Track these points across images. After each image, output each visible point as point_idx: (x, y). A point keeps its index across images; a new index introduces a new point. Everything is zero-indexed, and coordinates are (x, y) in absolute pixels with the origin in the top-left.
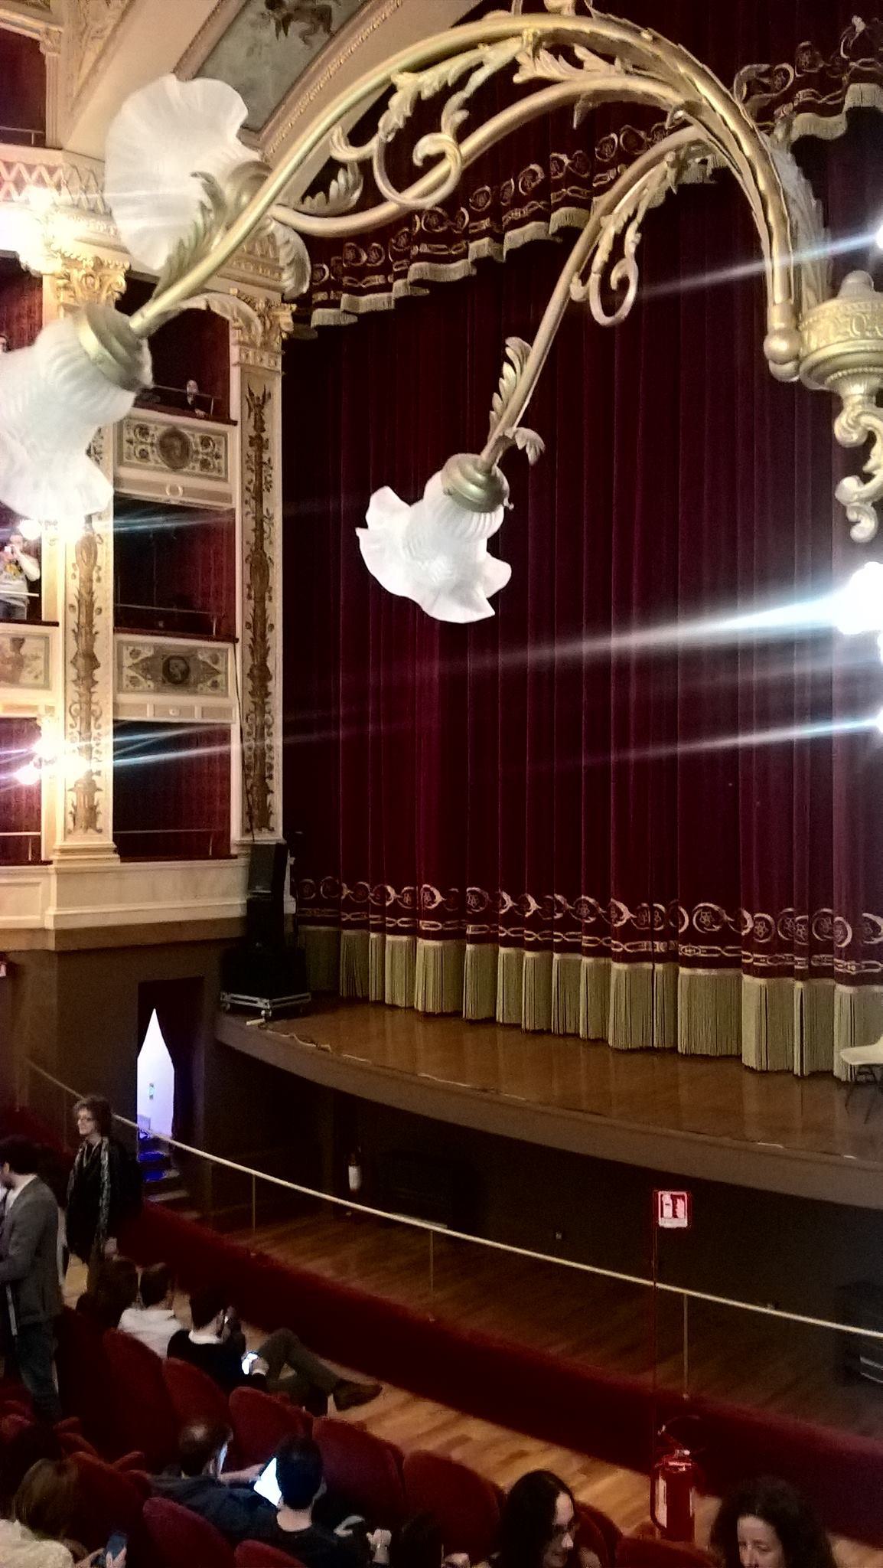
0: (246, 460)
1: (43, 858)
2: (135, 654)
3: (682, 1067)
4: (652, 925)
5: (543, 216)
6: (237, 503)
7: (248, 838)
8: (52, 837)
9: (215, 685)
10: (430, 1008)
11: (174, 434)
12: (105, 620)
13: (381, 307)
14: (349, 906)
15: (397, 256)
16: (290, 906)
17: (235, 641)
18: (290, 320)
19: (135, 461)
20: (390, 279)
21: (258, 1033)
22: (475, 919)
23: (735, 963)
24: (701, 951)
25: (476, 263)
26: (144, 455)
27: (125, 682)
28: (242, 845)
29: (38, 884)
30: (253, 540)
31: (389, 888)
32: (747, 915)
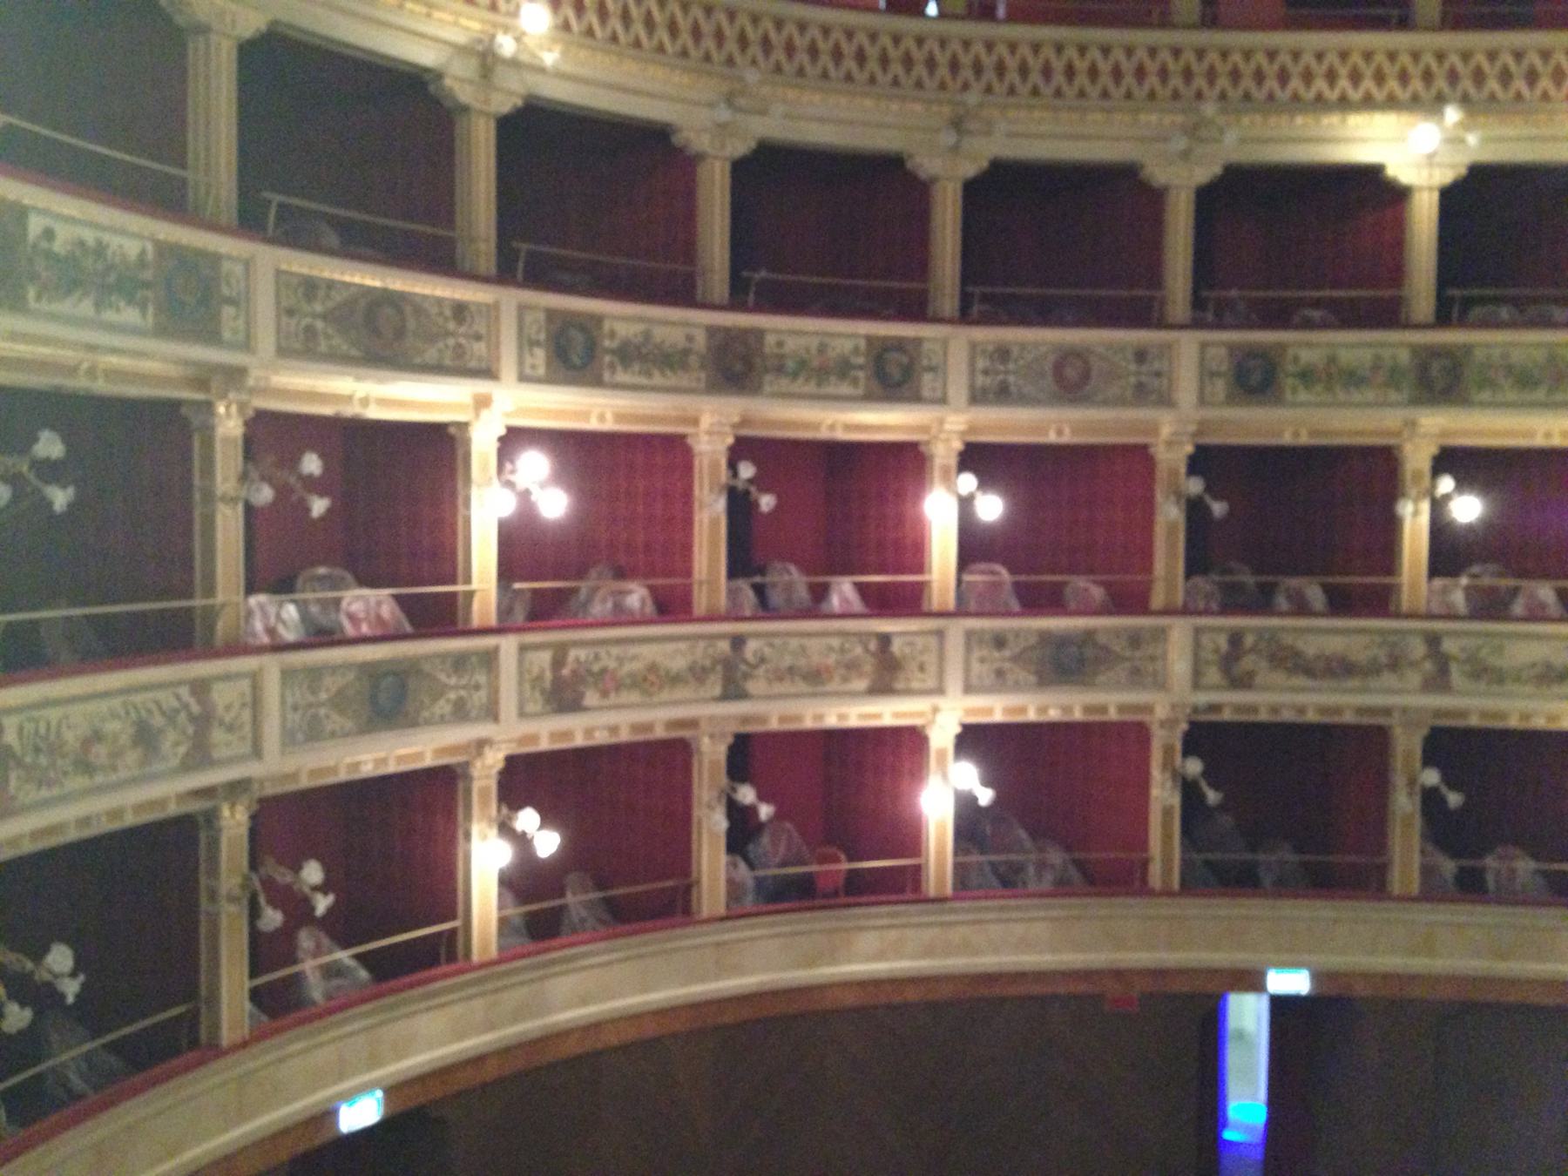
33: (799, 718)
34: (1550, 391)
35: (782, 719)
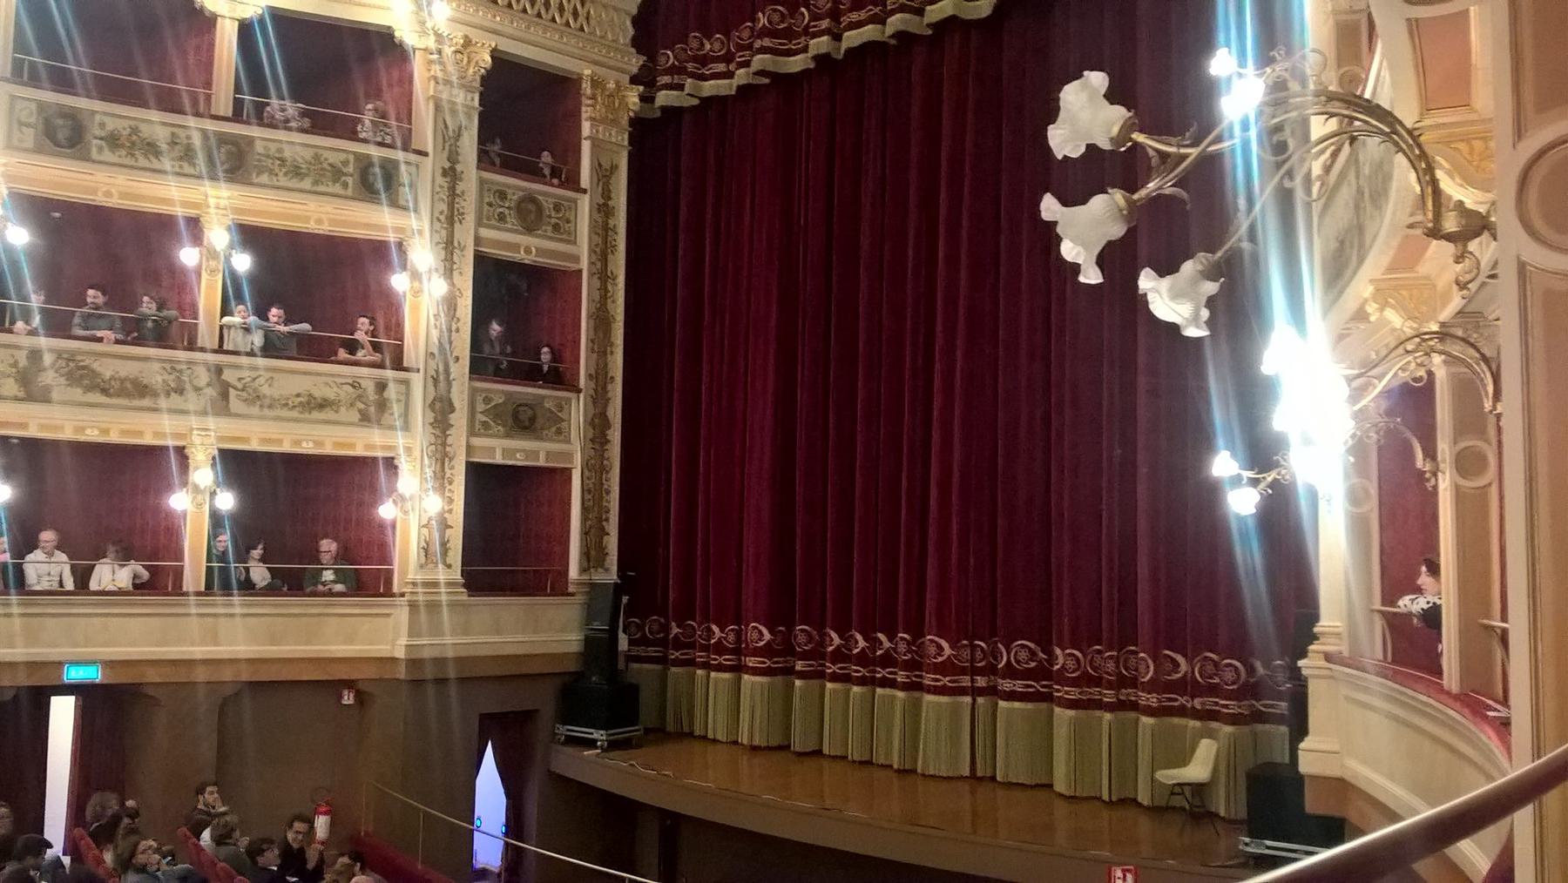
0: (593, 230)
1: (395, 589)
2: (487, 400)
3: (1000, 793)
4: (973, 660)
5: (881, 20)
6: (584, 265)
7: (585, 577)
8: (404, 572)
9: (559, 432)
10: (756, 742)
11: (531, 199)
12: (461, 370)
13: (724, 93)
14: (678, 644)
15: (741, 48)
16: (623, 643)
17: (579, 391)
18: (637, 100)
19: (493, 222)
20: (732, 67)
21: (597, 764)
22: (804, 656)
23: (1047, 698)
24: (1018, 686)
25: (816, 58)
26: (502, 218)
27: (477, 426)
28: (579, 584)
29: (388, 615)
30: (597, 298)
31: (714, 627)
32: (1058, 651)
33: (352, 446)
34: (316, 183)
35: (337, 445)
